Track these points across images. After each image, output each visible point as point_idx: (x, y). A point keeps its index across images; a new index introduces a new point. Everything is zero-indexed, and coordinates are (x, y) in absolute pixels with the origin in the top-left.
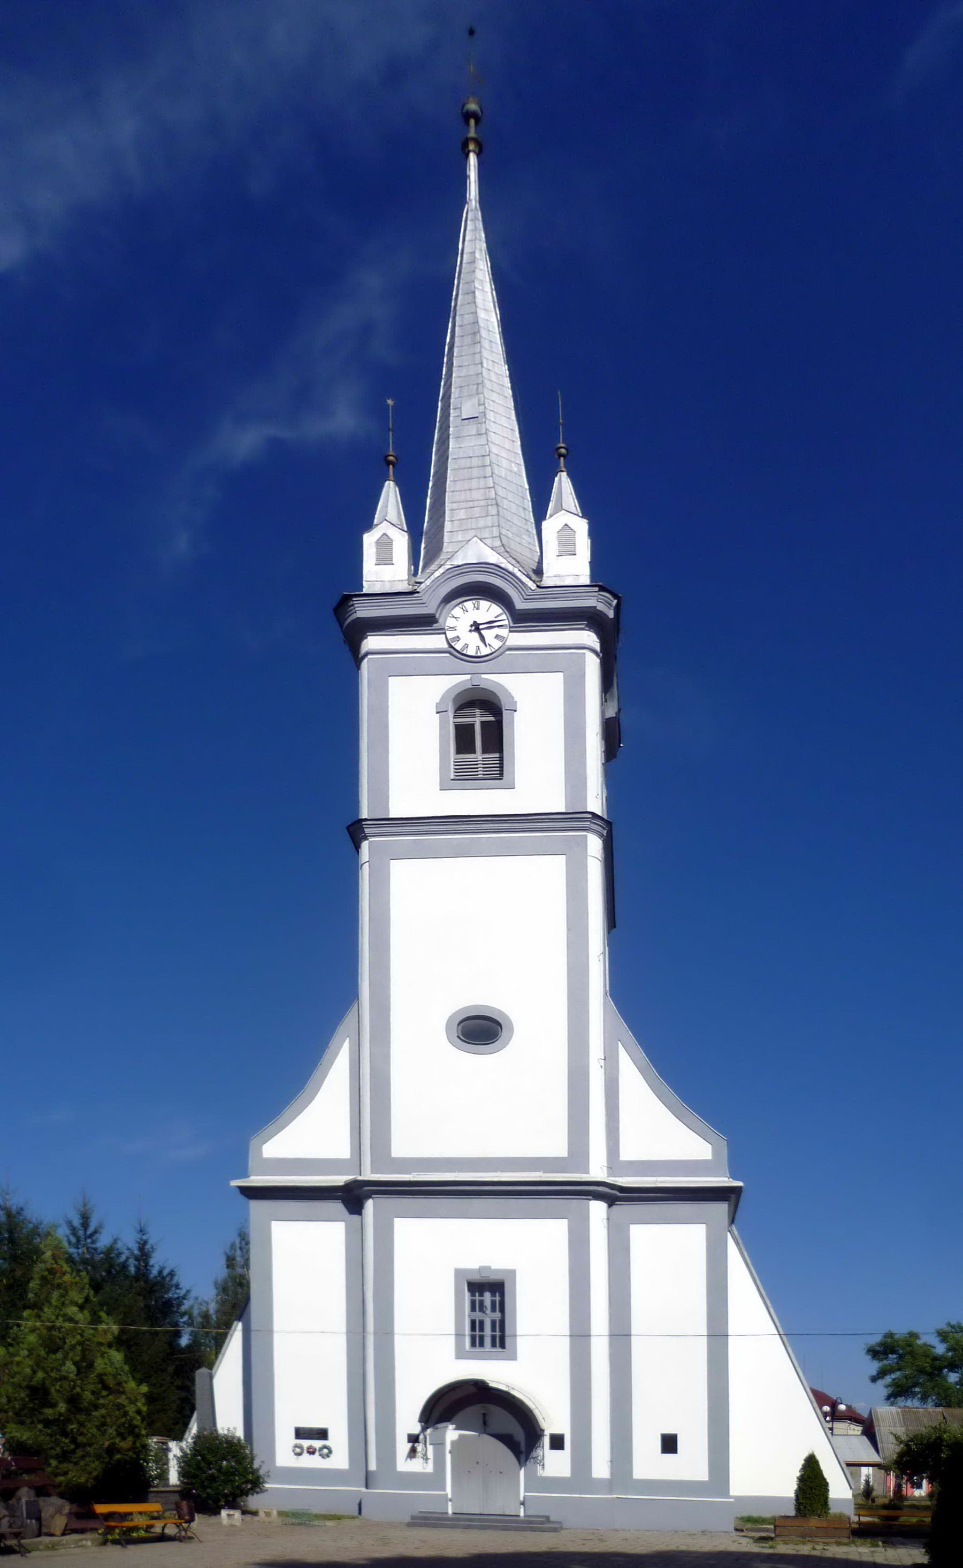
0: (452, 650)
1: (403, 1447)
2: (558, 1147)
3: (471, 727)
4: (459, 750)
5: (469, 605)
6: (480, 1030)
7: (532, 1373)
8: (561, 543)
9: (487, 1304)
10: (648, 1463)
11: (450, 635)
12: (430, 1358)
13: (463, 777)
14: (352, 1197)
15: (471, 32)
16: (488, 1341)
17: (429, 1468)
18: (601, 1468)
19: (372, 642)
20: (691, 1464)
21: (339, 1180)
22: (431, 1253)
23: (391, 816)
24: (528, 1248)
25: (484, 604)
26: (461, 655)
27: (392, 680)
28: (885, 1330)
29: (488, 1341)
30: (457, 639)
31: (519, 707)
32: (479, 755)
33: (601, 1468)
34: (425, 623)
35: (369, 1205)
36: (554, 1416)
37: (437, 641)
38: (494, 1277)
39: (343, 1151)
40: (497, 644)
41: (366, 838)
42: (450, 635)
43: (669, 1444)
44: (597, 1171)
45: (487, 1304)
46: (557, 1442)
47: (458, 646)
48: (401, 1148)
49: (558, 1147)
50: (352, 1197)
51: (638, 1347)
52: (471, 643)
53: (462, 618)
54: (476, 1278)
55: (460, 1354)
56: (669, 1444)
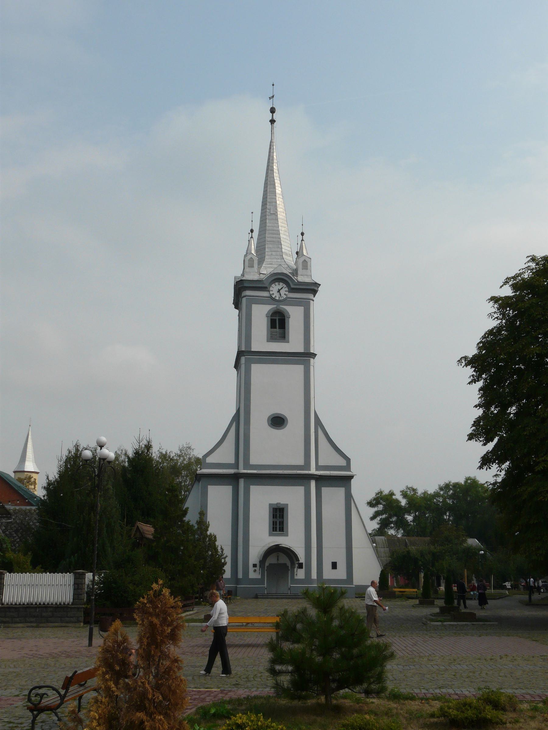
0: (271, 297)
1: (251, 569)
2: (300, 461)
3: (275, 320)
4: (271, 328)
5: (277, 283)
6: (278, 421)
7: (294, 540)
8: (303, 266)
9: (278, 518)
10: (328, 574)
11: (271, 293)
12: (261, 538)
13: (271, 338)
14: (233, 479)
15: (273, 85)
16: (278, 529)
17: (259, 577)
18: (314, 576)
19: (248, 293)
20: (341, 573)
21: (232, 471)
22: (262, 498)
23: (253, 349)
24: (291, 497)
25: (281, 284)
26: (274, 299)
27: (253, 305)
28: (377, 490)
29: (278, 529)
30: (273, 294)
31: (291, 317)
32: (277, 330)
33: (314, 576)
34: (265, 289)
35: (242, 482)
36: (302, 560)
37: (265, 294)
38: (281, 507)
39: (231, 460)
40: (285, 297)
41: (244, 356)
42: (271, 293)
43: (334, 566)
44: (313, 471)
45: (278, 518)
46: (300, 566)
47: (273, 296)
48: (253, 461)
49: (300, 461)
50: (233, 479)
51: (324, 550)
52: (276, 295)
53: (274, 289)
54: (276, 507)
55: (270, 535)
56: (334, 566)
